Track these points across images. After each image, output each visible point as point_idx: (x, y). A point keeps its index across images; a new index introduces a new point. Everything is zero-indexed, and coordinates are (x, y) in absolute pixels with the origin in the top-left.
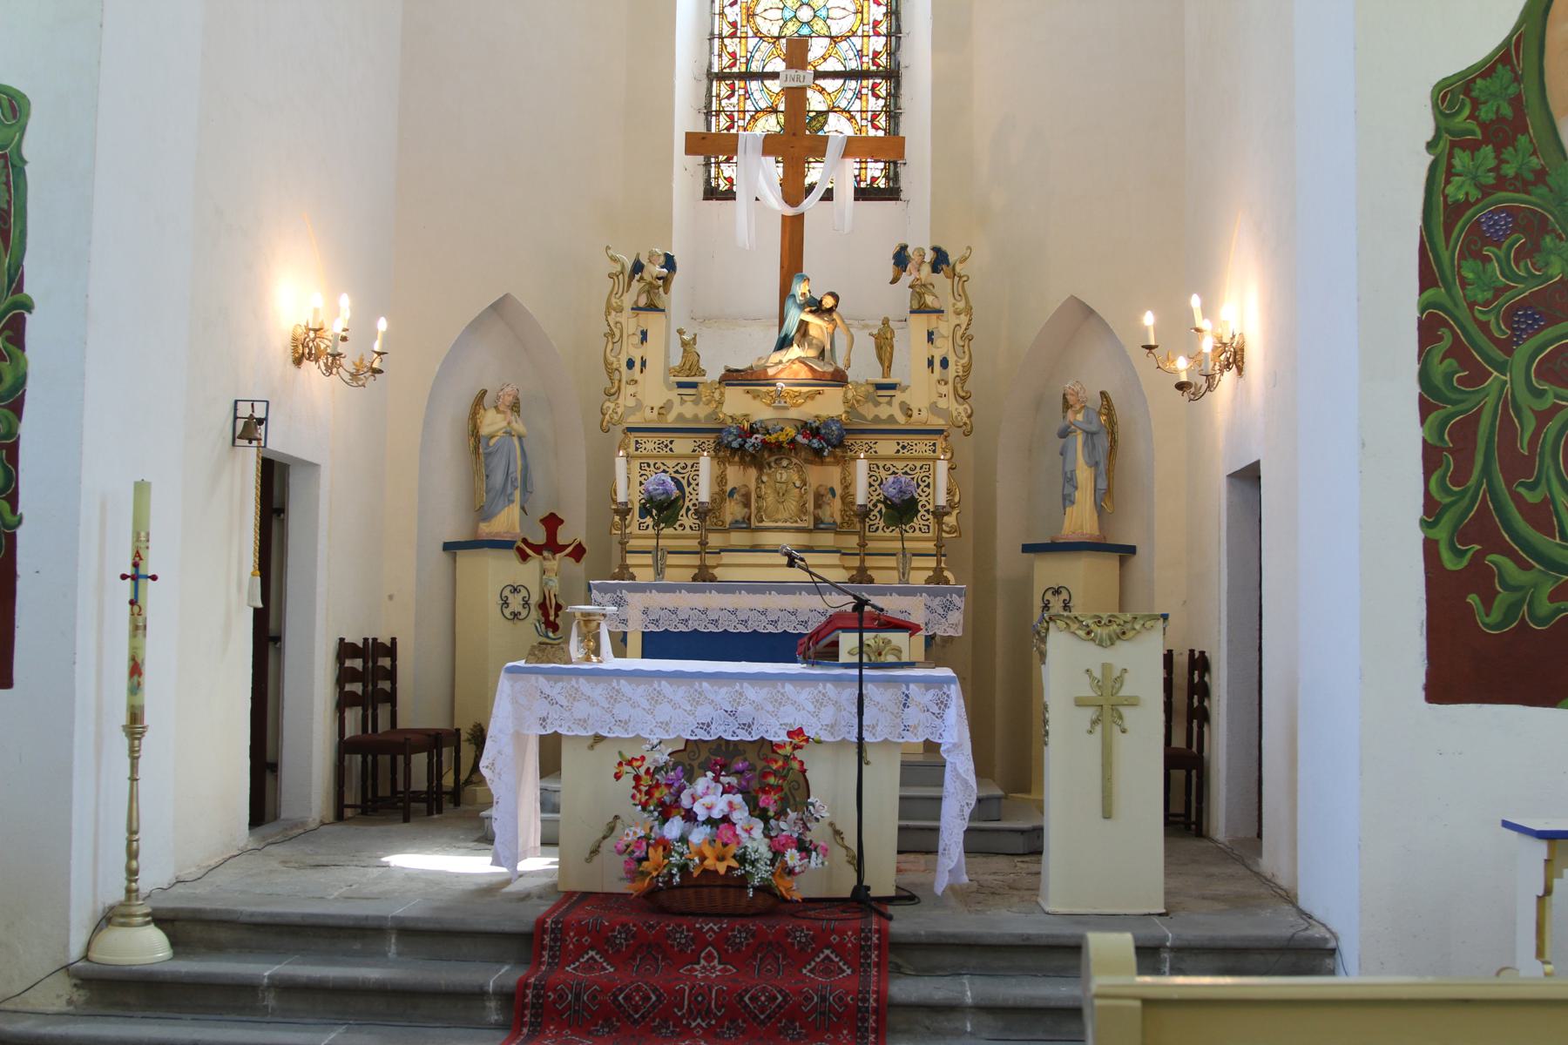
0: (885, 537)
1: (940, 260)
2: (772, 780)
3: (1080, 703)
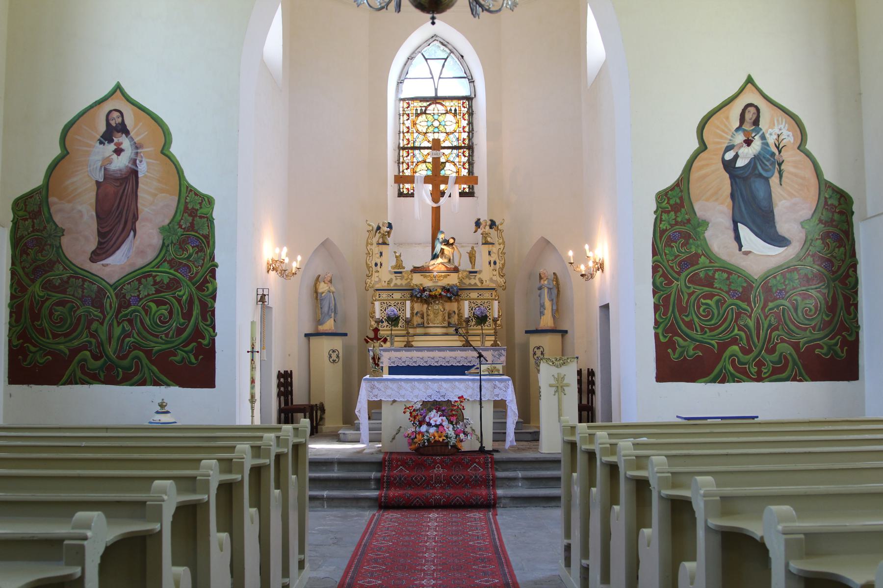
0: (475, 329)
1: (493, 224)
2: (454, 413)
3: (551, 386)
